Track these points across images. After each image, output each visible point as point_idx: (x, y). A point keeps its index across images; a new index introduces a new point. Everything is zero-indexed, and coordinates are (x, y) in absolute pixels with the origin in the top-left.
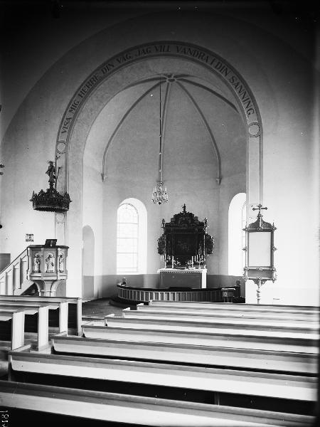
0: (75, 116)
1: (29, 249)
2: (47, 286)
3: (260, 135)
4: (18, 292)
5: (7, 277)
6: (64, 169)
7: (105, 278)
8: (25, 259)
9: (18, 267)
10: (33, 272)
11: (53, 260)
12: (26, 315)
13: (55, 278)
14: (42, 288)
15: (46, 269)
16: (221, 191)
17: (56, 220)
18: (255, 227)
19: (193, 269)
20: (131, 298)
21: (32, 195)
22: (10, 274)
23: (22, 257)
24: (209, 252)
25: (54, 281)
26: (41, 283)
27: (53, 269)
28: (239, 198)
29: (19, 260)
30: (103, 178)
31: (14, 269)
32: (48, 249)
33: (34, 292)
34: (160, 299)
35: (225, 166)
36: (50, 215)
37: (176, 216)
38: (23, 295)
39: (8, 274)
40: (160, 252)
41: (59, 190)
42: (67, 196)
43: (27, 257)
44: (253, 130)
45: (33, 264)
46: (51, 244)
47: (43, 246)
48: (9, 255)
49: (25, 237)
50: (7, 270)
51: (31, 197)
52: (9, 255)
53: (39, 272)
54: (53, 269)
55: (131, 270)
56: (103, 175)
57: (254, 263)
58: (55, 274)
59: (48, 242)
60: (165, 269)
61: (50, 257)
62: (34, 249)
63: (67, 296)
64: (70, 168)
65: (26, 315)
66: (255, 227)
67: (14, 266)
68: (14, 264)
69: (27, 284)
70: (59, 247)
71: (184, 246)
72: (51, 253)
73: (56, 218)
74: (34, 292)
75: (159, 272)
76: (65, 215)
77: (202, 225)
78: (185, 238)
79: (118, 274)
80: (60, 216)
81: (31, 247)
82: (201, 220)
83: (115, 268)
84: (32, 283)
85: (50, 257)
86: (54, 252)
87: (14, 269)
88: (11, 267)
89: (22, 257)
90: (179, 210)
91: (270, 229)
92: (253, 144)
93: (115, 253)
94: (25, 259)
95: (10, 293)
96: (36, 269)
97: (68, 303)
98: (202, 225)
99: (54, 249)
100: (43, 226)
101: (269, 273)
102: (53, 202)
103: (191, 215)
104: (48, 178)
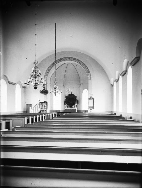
0: (49, 72)
3: (91, 79)
11: (45, 106)
12: (6, 122)
16: (80, 88)
18: (90, 99)
19: (74, 108)
24: (78, 104)
28: (85, 90)
34: (48, 119)
35: (81, 82)
37: (69, 94)
40: (65, 104)
43: (39, 105)
44: (89, 78)
46: (45, 102)
56: (50, 84)
57: (90, 106)
59: (45, 101)
60: (67, 108)
65: (6, 122)
66: (90, 99)
71: (71, 103)
72: (45, 104)
75: (65, 109)
77: (76, 97)
78: (71, 100)
82: (75, 96)
84: (40, 111)
90: (70, 93)
91: (93, 99)
92: (89, 81)
94: (38, 106)
95: (34, 112)
97: (5, 121)
98: (76, 97)
100: (43, 98)
101: (93, 108)
102: (44, 92)
103: (73, 94)
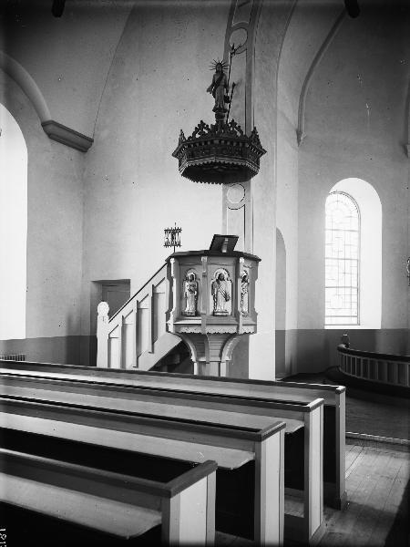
1: (172, 261)
2: (214, 347)
4: (148, 362)
5: (124, 327)
6: (242, 89)
7: (301, 334)
8: (163, 289)
9: (147, 305)
10: (182, 315)
11: (227, 286)
13: (232, 330)
14: (201, 352)
15: (211, 310)
17: (226, 206)
20: (380, 378)
21: (177, 138)
22: (131, 321)
23: (154, 282)
25: (229, 336)
26: (201, 340)
27: (226, 307)
29: (149, 290)
30: (299, 140)
31: (139, 311)
32: (214, 260)
33: (177, 360)
36: (214, 191)
38: (158, 369)
39: (127, 321)
41: (235, 113)
42: (255, 136)
45: (181, 297)
46: (222, 247)
47: (205, 253)
48: (127, 282)
49: (163, 238)
50: (124, 312)
51: (175, 146)
52: (127, 282)
53: (197, 314)
54: (226, 307)
55: (346, 321)
56: (299, 133)
58: (234, 322)
61: (221, 278)
62: (185, 260)
63: (251, 377)
64: (256, 84)
67: (138, 303)
68: (139, 298)
69: (167, 343)
70: (240, 254)
72: (221, 268)
73: (225, 198)
74: (177, 360)
76: (247, 189)
79: (327, 328)
80: (235, 193)
81: (178, 257)
83: (322, 317)
84: (177, 341)
85: (221, 278)
86: (231, 269)
87: (139, 311)
88: (132, 305)
89: (154, 282)
93: (321, 289)
94: (163, 289)
96: (189, 308)
99: (231, 261)
100: (202, 212)
102: (220, 156)
104: (212, 102)
